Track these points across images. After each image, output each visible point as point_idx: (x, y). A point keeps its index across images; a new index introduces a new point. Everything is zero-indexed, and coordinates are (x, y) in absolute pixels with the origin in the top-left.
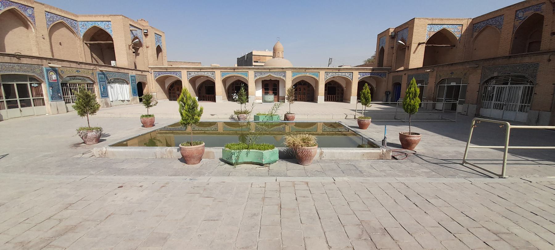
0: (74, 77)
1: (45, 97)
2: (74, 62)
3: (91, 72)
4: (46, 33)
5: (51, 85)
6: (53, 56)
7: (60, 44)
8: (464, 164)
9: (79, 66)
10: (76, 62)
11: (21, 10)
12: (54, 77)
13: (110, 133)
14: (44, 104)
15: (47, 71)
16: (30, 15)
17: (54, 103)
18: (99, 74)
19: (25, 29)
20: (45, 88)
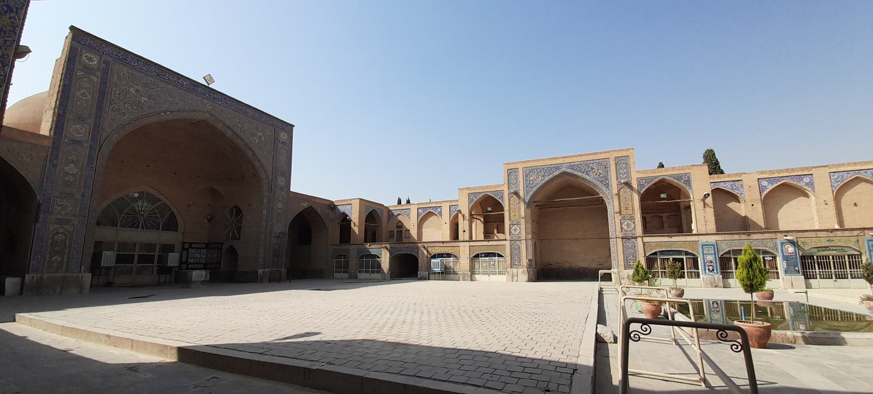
0: (826, 248)
1: (779, 271)
2: (823, 230)
3: (854, 239)
4: (830, 197)
5: (786, 258)
6: (841, 222)
7: (855, 205)
8: (185, 252)
9: (831, 235)
10: (827, 230)
11: (795, 183)
12: (791, 249)
13: (322, 331)
14: (778, 278)
15: (782, 244)
16: (807, 184)
17: (788, 277)
18: (868, 241)
19: (802, 199)
20: (781, 264)
